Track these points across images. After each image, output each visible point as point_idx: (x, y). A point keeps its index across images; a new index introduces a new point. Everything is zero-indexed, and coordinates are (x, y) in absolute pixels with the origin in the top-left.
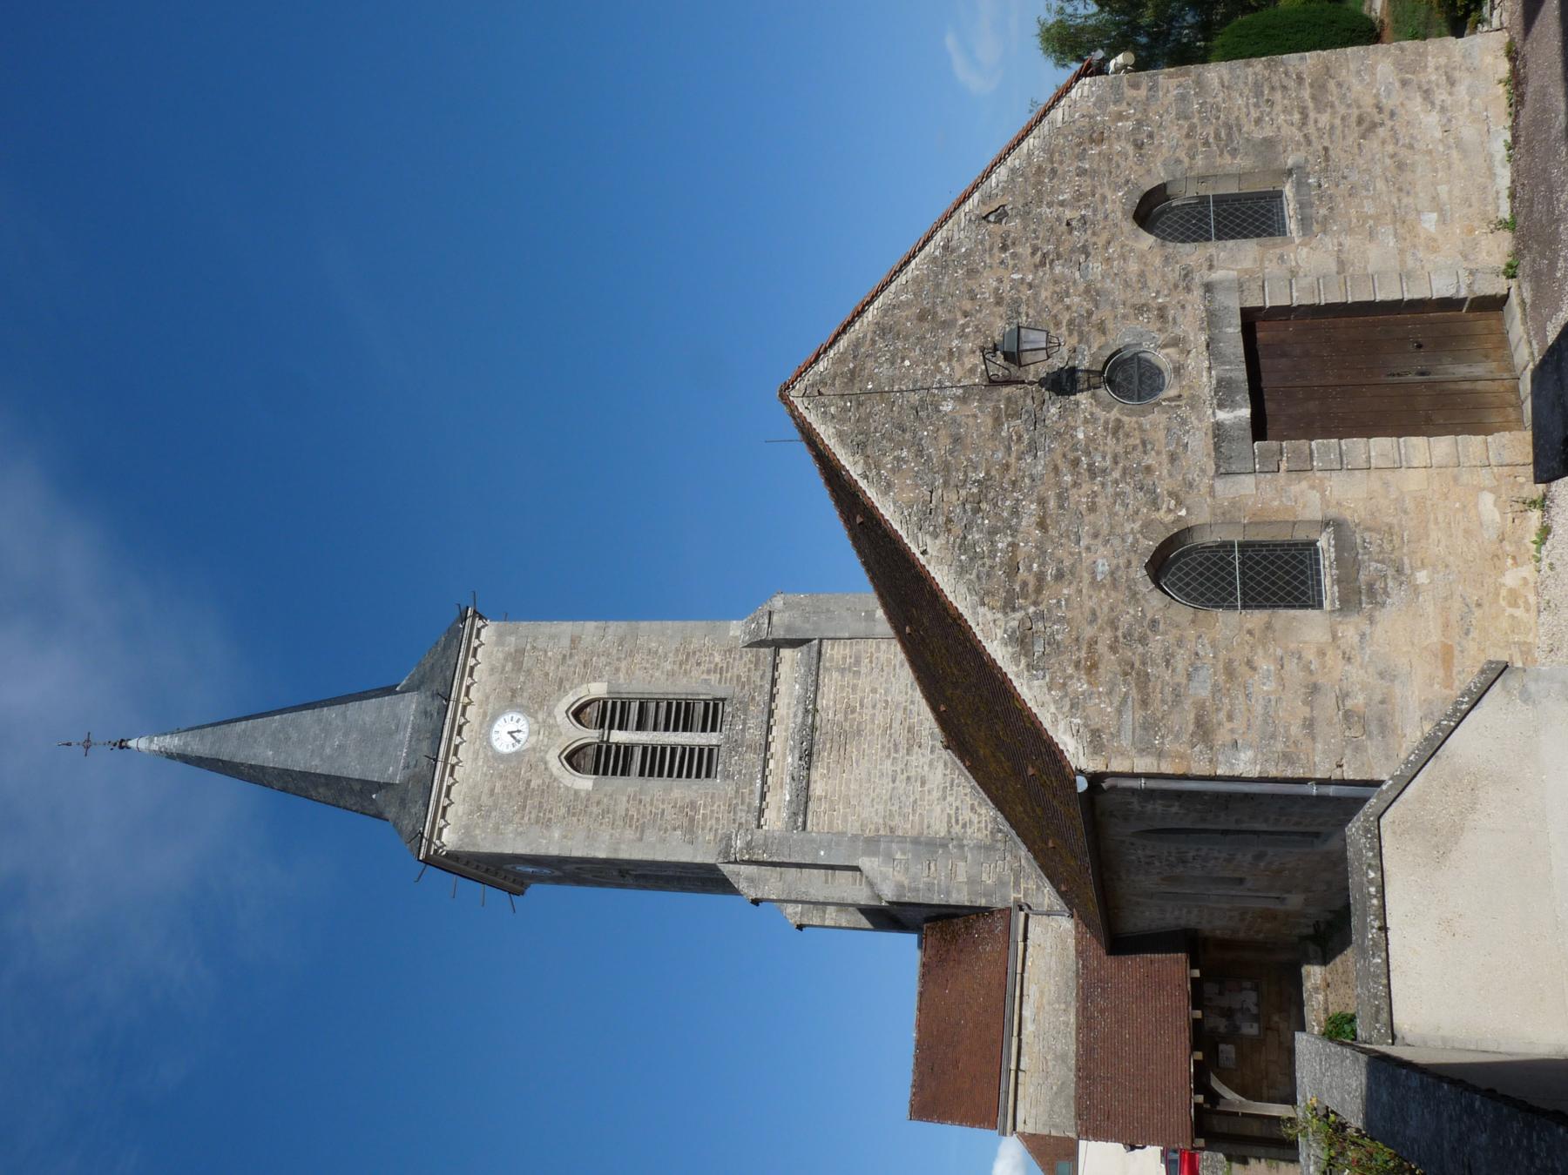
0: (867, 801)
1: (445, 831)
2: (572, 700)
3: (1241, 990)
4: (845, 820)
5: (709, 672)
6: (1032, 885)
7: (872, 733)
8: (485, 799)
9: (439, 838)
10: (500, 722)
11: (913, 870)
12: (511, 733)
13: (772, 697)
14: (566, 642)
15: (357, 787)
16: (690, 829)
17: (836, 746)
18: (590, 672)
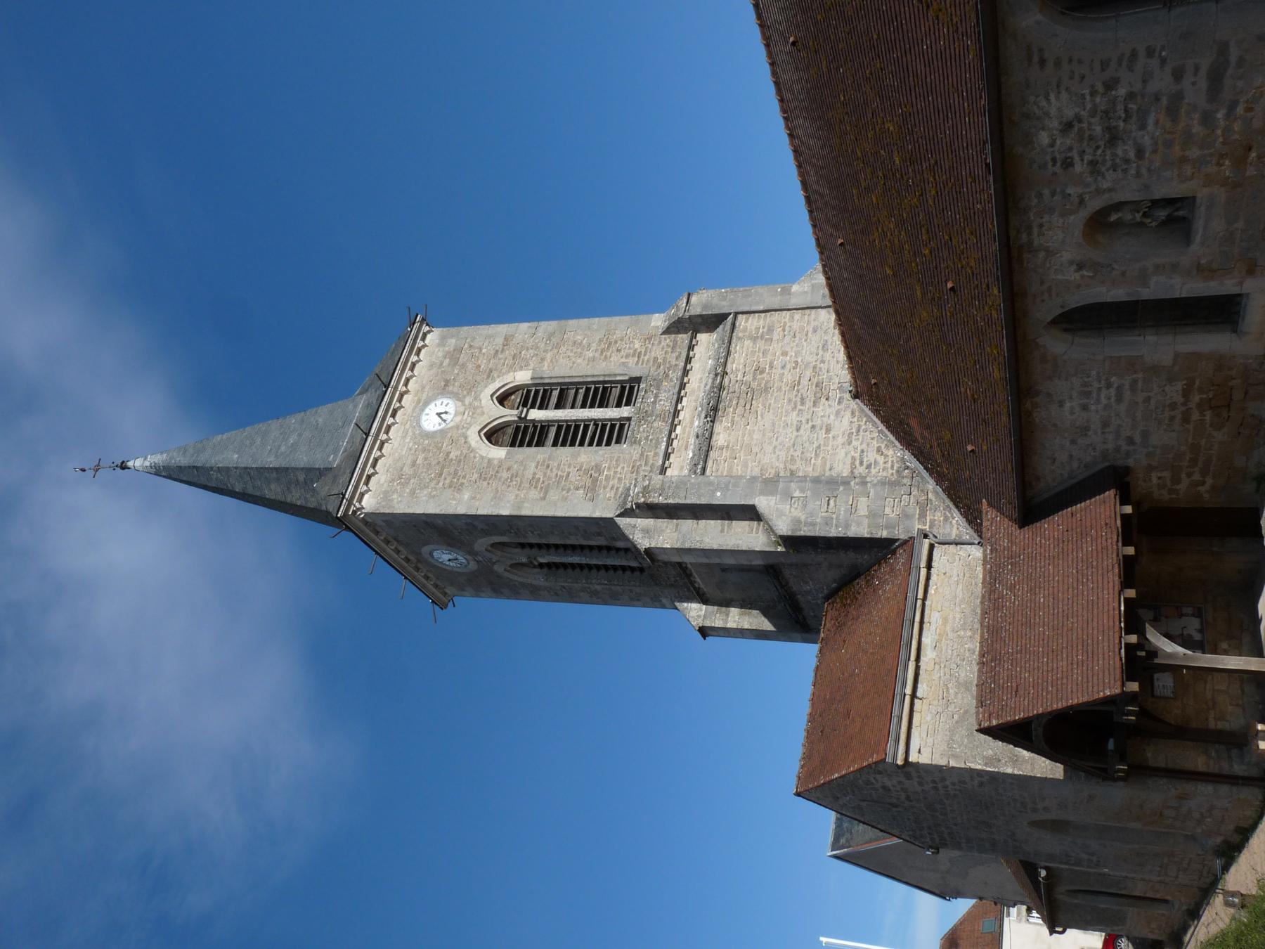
0: (768, 449)
1: (366, 496)
2: (498, 385)
3: (1181, 615)
4: (745, 465)
5: (627, 356)
6: (939, 516)
7: (780, 389)
8: (407, 470)
9: (360, 501)
10: (432, 406)
11: (811, 506)
12: (439, 414)
13: (686, 372)
14: (500, 340)
15: (301, 477)
16: (592, 490)
17: (742, 402)
18: (518, 362)
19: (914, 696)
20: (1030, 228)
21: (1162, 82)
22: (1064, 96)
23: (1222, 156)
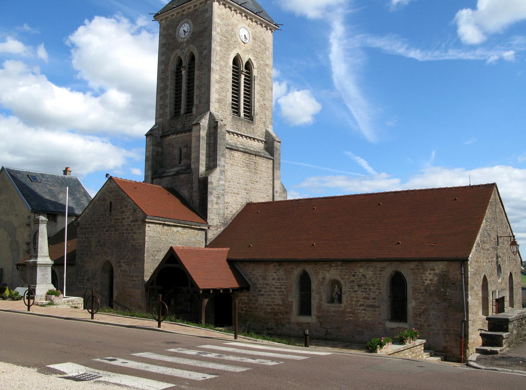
19: (164, 225)
20: (337, 266)
21: (373, 295)
22: (372, 275)
23: (352, 309)
